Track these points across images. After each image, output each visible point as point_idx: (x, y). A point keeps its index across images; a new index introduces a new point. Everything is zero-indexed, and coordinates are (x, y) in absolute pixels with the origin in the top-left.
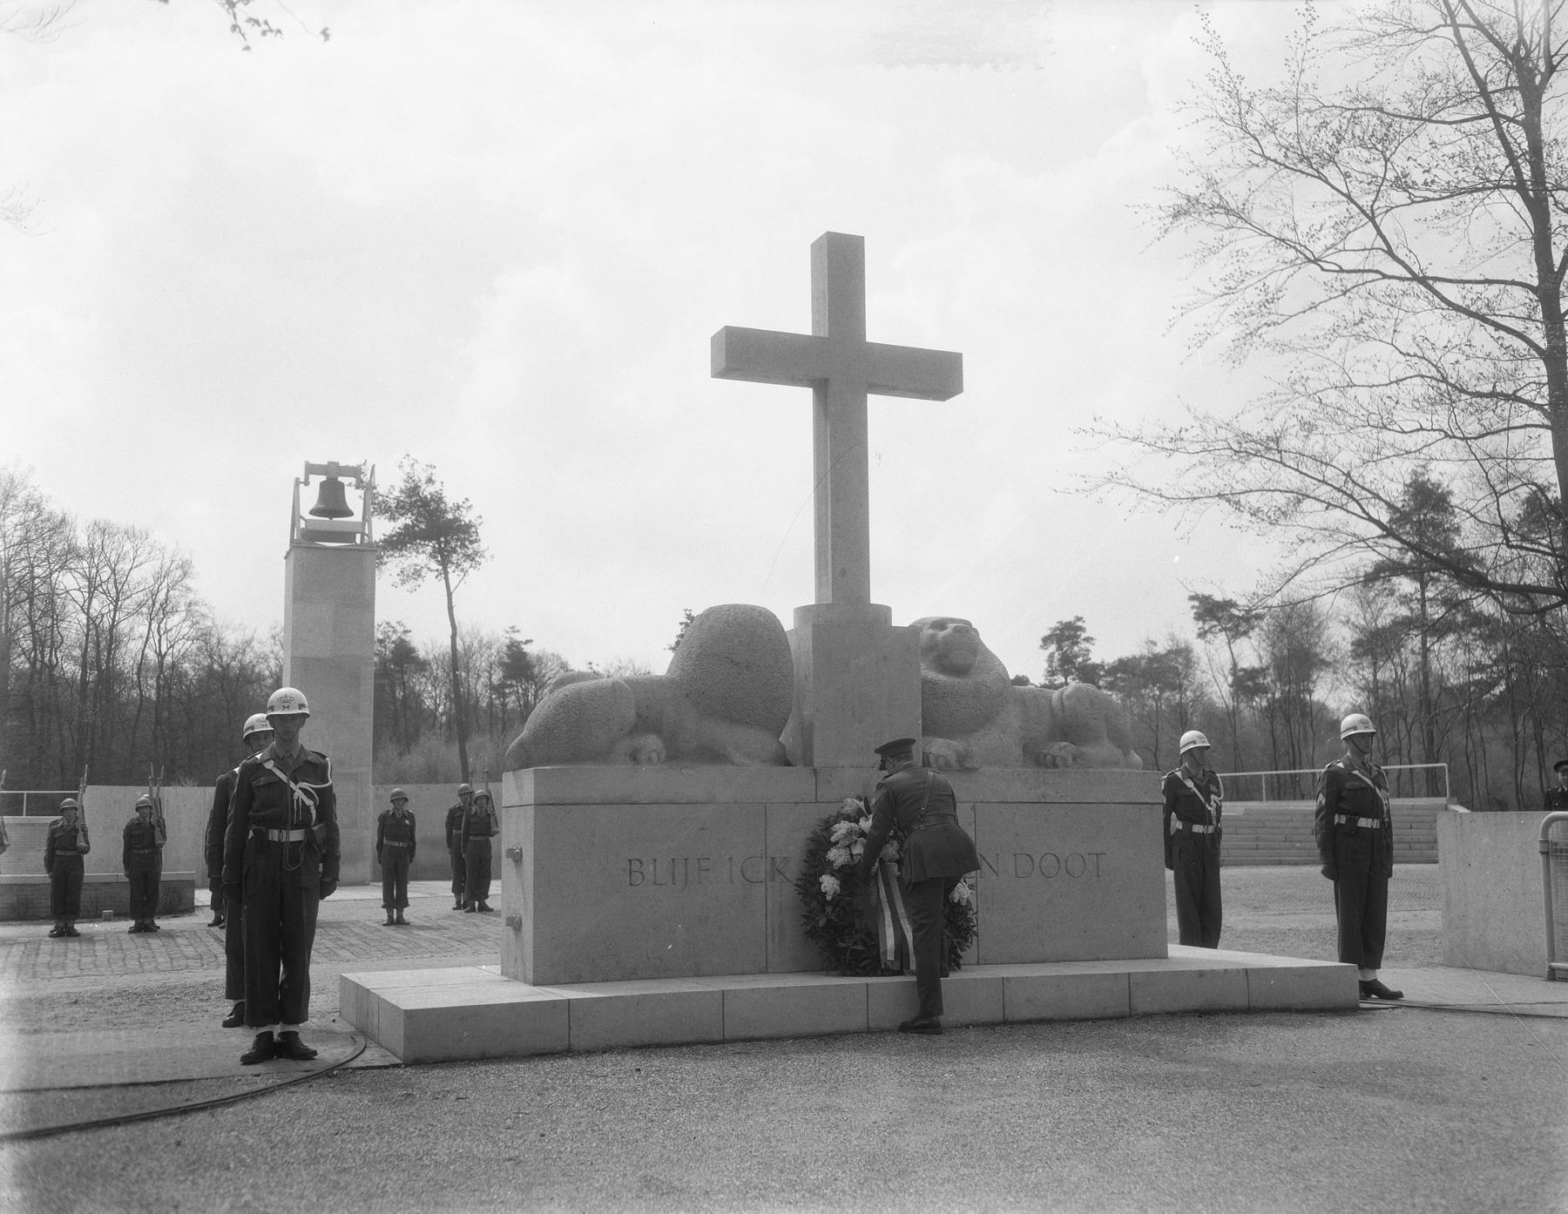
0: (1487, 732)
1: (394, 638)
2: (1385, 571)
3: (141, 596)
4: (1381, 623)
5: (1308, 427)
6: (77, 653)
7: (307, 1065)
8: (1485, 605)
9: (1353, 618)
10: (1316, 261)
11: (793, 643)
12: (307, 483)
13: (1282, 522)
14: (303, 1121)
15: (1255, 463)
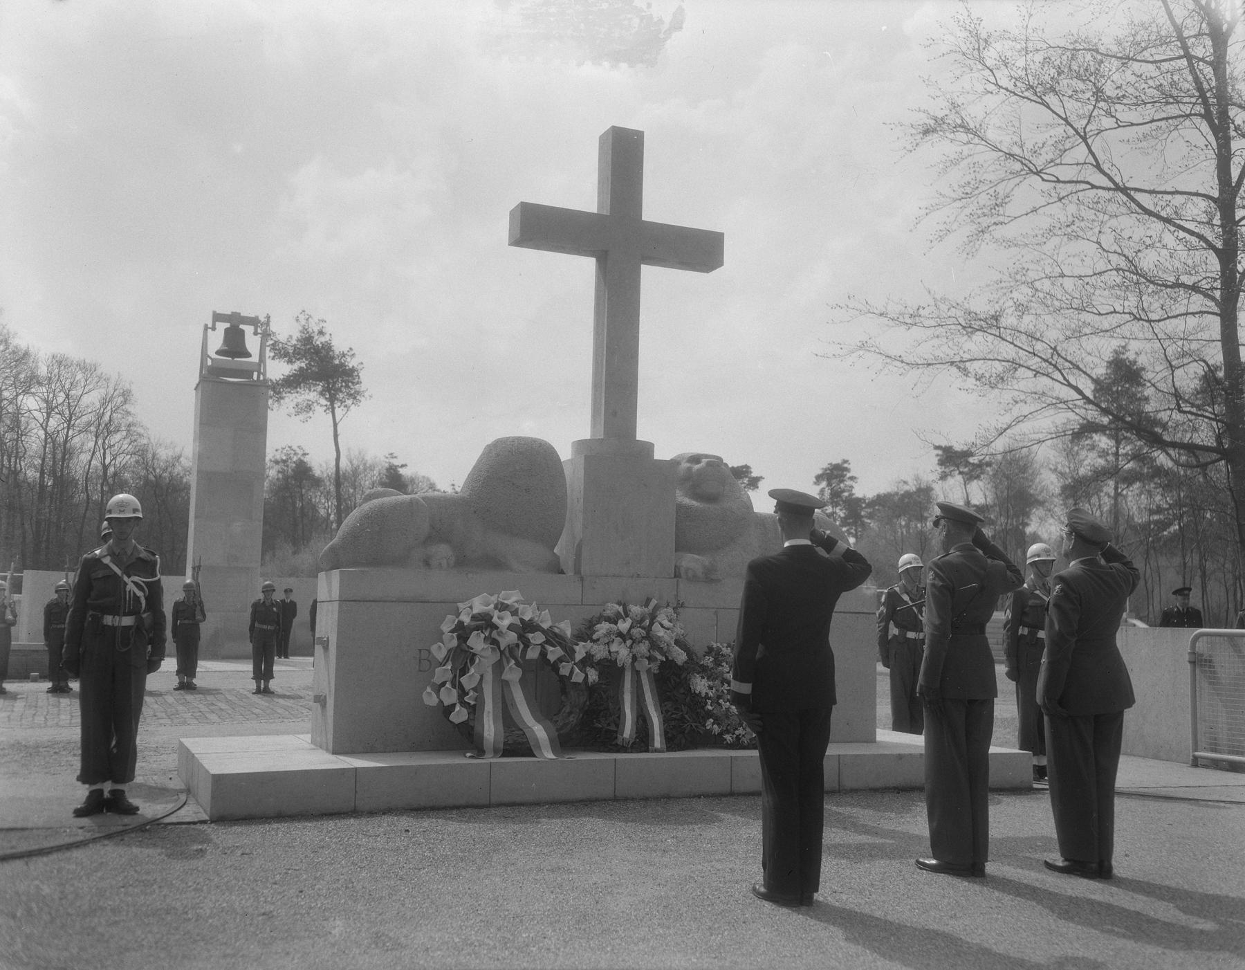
0: (1163, 561)
1: (295, 459)
2: (1089, 428)
3: (91, 417)
4: (1082, 471)
5: (1022, 309)
6: (38, 462)
7: (127, 820)
8: (1162, 459)
9: (1060, 467)
10: (1038, 173)
11: (568, 471)
12: (214, 329)
13: (1000, 386)
14: (99, 874)
15: (978, 336)
